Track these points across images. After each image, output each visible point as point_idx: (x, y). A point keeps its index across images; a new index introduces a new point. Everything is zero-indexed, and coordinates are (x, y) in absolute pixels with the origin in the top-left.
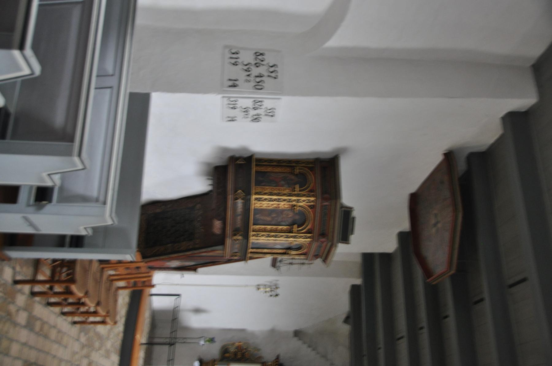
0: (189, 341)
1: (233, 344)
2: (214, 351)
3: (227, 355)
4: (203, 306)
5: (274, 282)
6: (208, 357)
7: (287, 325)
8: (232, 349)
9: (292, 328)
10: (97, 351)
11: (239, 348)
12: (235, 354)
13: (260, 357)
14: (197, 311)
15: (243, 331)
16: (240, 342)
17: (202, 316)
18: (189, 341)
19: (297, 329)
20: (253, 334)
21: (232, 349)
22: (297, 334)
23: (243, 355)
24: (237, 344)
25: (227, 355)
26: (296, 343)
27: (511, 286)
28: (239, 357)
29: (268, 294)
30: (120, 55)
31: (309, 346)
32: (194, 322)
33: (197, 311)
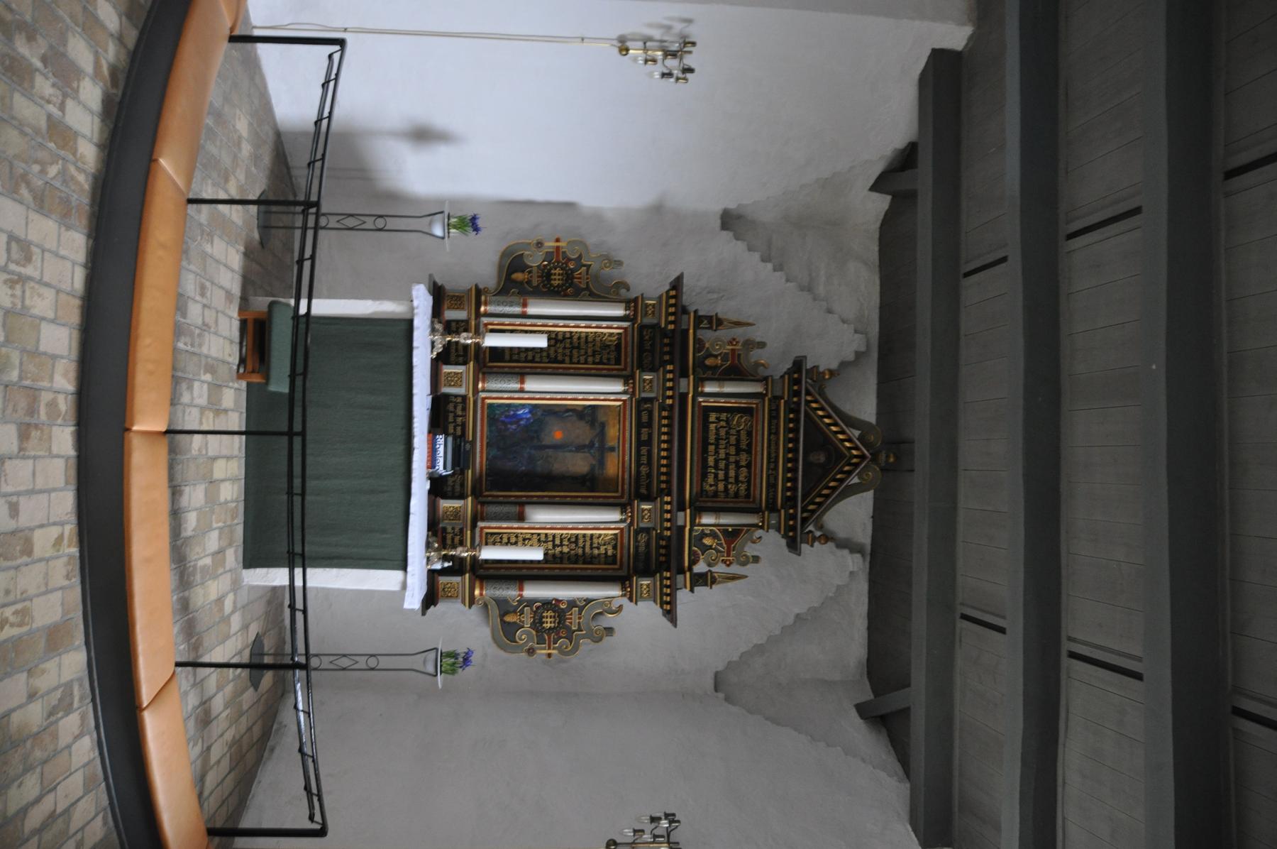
0: (391, 224)
1: (539, 244)
2: (477, 262)
3: (518, 276)
4: (439, 119)
5: (678, 27)
6: (457, 281)
7: (702, 193)
8: (535, 260)
9: (718, 208)
10: (754, 542)
11: (557, 258)
12: (546, 274)
13: (623, 285)
14: (423, 135)
15: (569, 206)
16: (558, 240)
17: (440, 155)
18: (391, 224)
19: (732, 205)
20: (597, 217)
21: (535, 260)
22: (730, 221)
23: (569, 276)
24: (550, 244)
25: (518, 276)
26: (727, 247)
27: (967, 275)
28: (556, 283)
29: (657, 70)
30: (598, 568)
31: (765, 259)
32: (418, 175)
33: (423, 135)
